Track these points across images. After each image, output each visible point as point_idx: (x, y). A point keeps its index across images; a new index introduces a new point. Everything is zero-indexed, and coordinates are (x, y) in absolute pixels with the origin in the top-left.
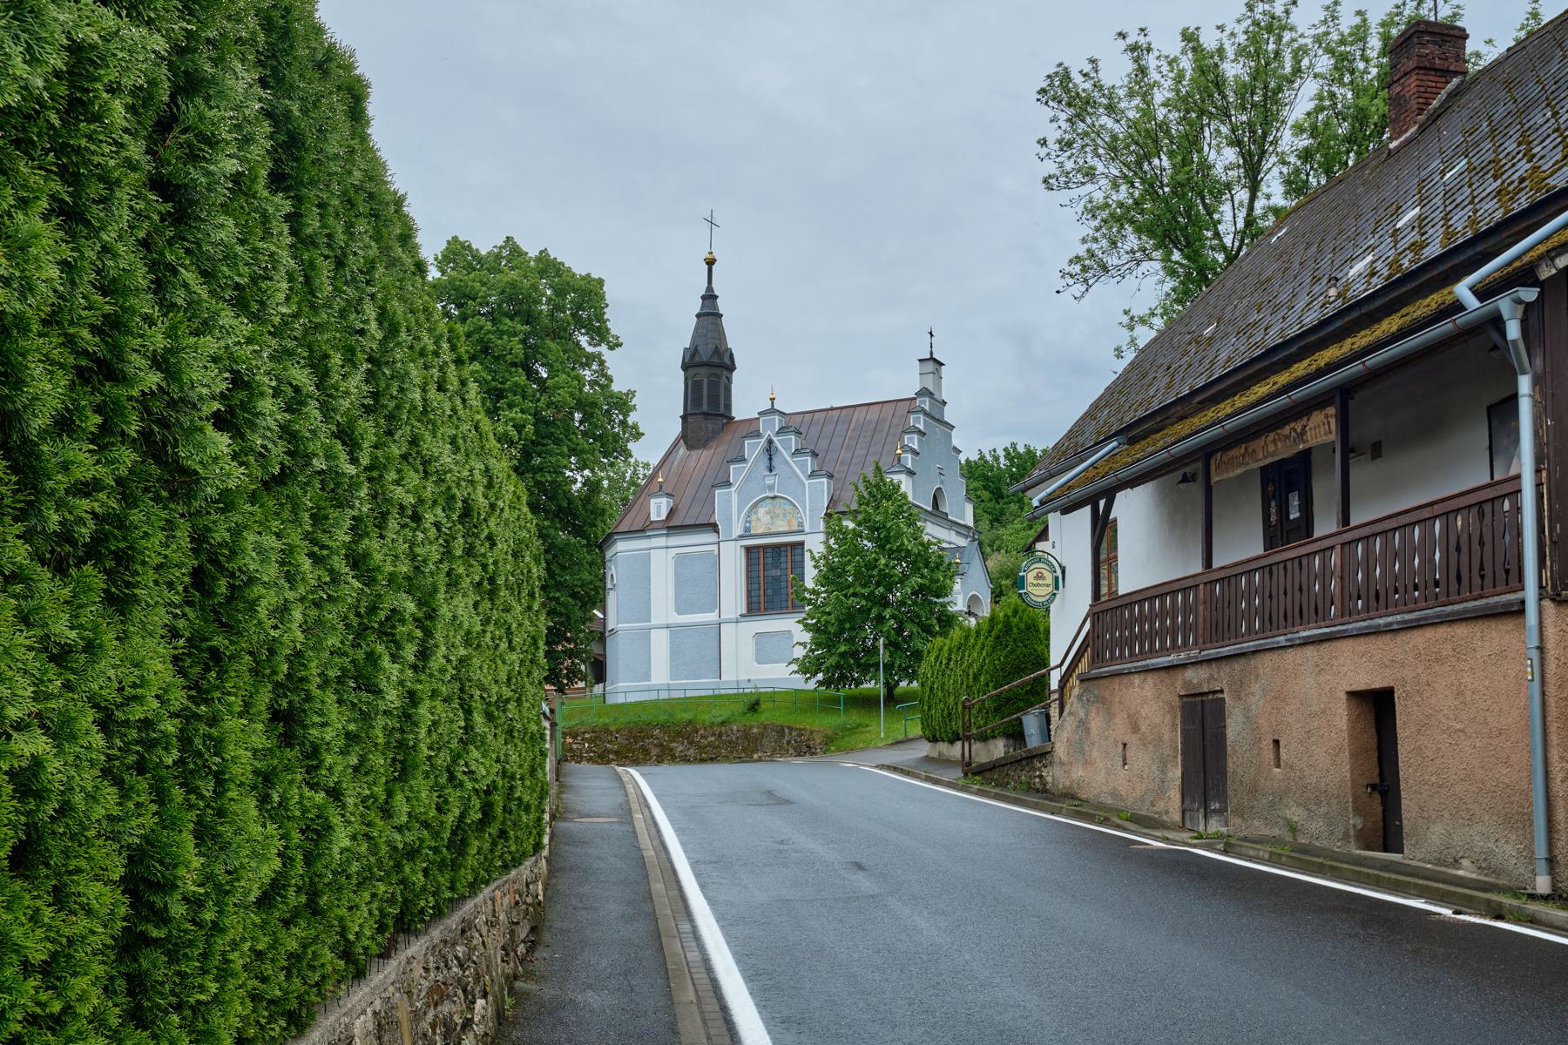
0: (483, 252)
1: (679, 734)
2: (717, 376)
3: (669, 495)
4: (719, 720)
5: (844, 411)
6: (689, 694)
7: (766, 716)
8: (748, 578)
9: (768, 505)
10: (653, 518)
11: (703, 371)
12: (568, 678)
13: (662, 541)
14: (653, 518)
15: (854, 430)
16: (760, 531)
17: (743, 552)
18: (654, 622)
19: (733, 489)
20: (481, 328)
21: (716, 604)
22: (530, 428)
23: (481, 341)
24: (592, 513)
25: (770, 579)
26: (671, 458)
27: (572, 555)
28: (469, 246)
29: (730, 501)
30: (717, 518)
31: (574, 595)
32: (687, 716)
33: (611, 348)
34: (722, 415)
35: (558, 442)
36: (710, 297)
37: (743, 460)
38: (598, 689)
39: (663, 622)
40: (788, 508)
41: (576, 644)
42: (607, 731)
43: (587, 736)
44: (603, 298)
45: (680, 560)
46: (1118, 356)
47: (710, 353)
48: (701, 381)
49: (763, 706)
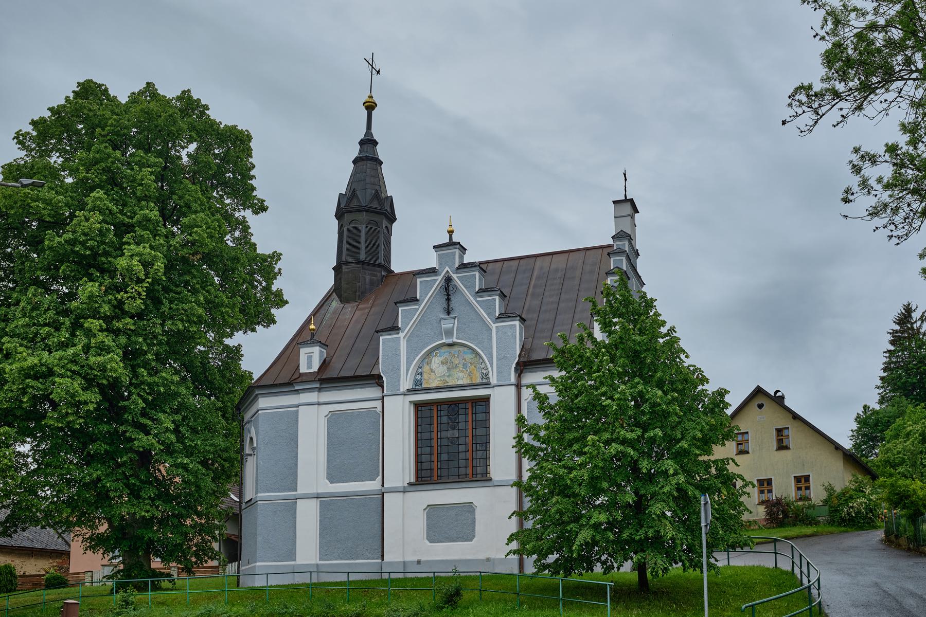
0: (123, 99)
2: (377, 224)
3: (323, 345)
6: (353, 577)
8: (417, 440)
9: (445, 353)
10: (303, 369)
11: (363, 217)
12: (196, 554)
13: (313, 397)
14: (303, 369)
15: (538, 278)
16: (434, 385)
18: (301, 490)
19: (401, 335)
21: (376, 469)
22: (159, 265)
23: (107, 170)
24: (230, 381)
25: (445, 442)
26: (322, 311)
28: (106, 90)
31: (204, 463)
34: (381, 266)
35: (194, 292)
36: (368, 142)
37: (414, 300)
38: (232, 568)
40: (469, 357)
41: (208, 519)
44: (248, 152)
45: (334, 420)
46: (846, 201)
48: (359, 228)
49: (466, 596)
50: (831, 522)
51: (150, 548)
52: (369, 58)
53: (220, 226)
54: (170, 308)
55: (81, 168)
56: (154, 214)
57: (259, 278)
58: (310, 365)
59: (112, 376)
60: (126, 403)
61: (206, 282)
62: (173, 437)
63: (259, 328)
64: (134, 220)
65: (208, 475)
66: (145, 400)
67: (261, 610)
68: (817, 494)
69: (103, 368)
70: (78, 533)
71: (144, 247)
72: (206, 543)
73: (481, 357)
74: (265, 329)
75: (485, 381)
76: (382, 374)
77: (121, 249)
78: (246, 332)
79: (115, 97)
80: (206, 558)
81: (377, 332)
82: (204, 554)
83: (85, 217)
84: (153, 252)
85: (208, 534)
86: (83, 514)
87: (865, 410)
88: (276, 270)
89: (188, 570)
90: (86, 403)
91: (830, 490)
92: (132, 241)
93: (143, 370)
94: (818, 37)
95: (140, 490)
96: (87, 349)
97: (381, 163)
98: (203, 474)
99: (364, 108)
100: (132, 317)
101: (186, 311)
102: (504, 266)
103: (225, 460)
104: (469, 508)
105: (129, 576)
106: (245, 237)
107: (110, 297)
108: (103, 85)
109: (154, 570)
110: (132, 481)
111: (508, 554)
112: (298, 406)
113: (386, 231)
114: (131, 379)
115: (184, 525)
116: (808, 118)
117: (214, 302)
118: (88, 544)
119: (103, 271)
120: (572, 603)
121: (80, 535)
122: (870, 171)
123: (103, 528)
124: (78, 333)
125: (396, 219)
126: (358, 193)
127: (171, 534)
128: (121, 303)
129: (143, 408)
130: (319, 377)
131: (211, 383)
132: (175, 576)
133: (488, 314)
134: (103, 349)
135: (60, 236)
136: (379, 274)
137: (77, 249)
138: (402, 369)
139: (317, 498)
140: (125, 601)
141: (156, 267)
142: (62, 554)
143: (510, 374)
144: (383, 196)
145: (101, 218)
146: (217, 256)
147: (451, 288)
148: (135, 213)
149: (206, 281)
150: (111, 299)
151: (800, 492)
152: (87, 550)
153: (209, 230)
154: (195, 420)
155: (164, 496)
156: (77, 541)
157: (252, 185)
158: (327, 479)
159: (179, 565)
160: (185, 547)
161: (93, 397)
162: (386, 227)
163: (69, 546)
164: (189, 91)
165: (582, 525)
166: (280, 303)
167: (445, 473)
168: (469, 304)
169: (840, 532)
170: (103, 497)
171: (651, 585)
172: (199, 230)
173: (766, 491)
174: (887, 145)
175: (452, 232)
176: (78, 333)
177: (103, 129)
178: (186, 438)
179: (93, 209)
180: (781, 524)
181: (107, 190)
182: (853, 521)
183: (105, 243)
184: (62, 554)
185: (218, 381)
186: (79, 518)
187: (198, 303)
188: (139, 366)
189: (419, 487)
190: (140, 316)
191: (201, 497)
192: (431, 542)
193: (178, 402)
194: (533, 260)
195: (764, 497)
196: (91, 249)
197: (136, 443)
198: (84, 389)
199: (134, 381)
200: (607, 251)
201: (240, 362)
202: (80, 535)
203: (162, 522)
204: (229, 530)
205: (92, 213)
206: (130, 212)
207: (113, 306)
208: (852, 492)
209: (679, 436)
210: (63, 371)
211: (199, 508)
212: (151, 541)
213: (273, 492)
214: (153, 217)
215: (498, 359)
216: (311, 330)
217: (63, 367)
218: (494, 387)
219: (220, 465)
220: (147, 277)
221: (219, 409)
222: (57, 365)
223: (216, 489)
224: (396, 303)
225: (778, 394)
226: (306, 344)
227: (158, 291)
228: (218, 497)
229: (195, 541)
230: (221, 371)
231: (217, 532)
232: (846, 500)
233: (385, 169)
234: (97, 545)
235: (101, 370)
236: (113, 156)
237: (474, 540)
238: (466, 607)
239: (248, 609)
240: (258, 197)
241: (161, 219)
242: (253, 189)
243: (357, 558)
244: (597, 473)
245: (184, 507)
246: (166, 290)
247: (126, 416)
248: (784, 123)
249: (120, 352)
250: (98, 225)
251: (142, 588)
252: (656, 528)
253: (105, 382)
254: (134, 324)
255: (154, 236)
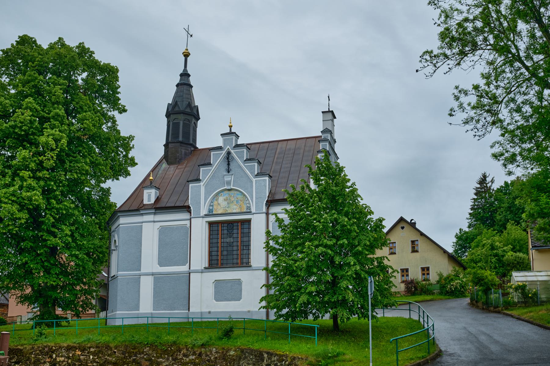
0: (45, 46)
1: (165, 352)
2: (189, 121)
3: (157, 188)
4: (200, 343)
5: (271, 144)
6: (172, 321)
7: (242, 342)
8: (210, 243)
9: (226, 195)
10: (146, 202)
11: (181, 117)
12: (82, 306)
13: (151, 218)
14: (146, 202)
15: (279, 153)
16: (220, 212)
17: (207, 224)
18: (143, 270)
19: (202, 184)
20: (36, 78)
21: (186, 259)
22: (64, 141)
23: (35, 86)
27: (89, 229)
28: (35, 41)
29: (200, 191)
30: (190, 202)
31: (88, 254)
32: (171, 338)
33: (120, 113)
34: (191, 145)
35: (84, 157)
36: (185, 75)
37: (209, 164)
38: (102, 315)
39: (150, 271)
40: (240, 197)
41: (89, 286)
42: (108, 347)
43: (92, 350)
45: (163, 231)
46: (451, 115)
47: (184, 106)
49: (236, 332)
50: (441, 293)
51: (56, 302)
52: (186, 28)
53: (99, 120)
54: (70, 166)
55: (20, 85)
56: (62, 112)
57: (121, 150)
58: (149, 200)
59: (35, 204)
60: (43, 219)
61: (91, 151)
62: (70, 239)
63: (121, 178)
64: (50, 115)
65: (90, 261)
66: (54, 218)
67: (119, 339)
68: (433, 277)
69: (30, 199)
70: (13, 293)
71: (56, 131)
72: (88, 300)
73: (246, 197)
74: (125, 179)
75: (248, 210)
76: (190, 205)
77: (42, 131)
78: (113, 180)
79: (40, 45)
80: (88, 309)
81: (188, 182)
82: (86, 306)
83: (22, 112)
84: (61, 134)
85: (89, 294)
86: (17, 282)
87: (460, 231)
88: (131, 146)
89: (78, 315)
90: (20, 219)
91: (440, 275)
92: (48, 127)
93: (53, 200)
94: (436, 25)
95: (50, 269)
96: (21, 188)
97: (192, 87)
98: (87, 261)
99: (183, 56)
100: (48, 170)
101: (79, 167)
102: (261, 146)
103: (100, 253)
104: (238, 282)
105: (43, 319)
106: (114, 126)
107: (35, 159)
108: (33, 38)
109: (57, 315)
110: (46, 264)
111: (260, 309)
112: (142, 223)
113: (194, 125)
114: (46, 206)
115: (75, 289)
116: (431, 68)
117: (95, 163)
118: (19, 300)
119: (31, 144)
120: (296, 336)
121: (15, 294)
122: (464, 99)
123: (28, 291)
124: (16, 179)
125: (200, 118)
126: (178, 103)
127: (68, 294)
128: (41, 162)
129: (53, 222)
130: (154, 207)
131: (92, 208)
132: (70, 319)
133: (251, 173)
134: (30, 188)
135: (6, 123)
136: (189, 149)
137: (16, 131)
138: (201, 203)
139: (152, 275)
140: (40, 333)
141: (62, 142)
142: (4, 305)
143: (263, 207)
144: (193, 106)
145: (31, 113)
146: (98, 137)
147: (230, 158)
148: (51, 111)
149: (91, 151)
150: (36, 160)
151: (424, 276)
152: (18, 303)
153: (93, 122)
154: (83, 230)
155: (65, 273)
156: (13, 298)
157: (118, 97)
158: (158, 264)
159: (72, 313)
160: (76, 302)
161: (24, 216)
162: (194, 123)
163: (8, 301)
164: (83, 43)
165: (302, 293)
166: (133, 164)
167: (225, 262)
168: (240, 167)
169: (446, 299)
170: (29, 272)
171: (340, 327)
172: (87, 122)
173: (405, 275)
174: (473, 85)
175: (231, 126)
176: (16, 179)
177: (33, 63)
178: (78, 240)
179: (26, 108)
180: (413, 294)
181: (35, 98)
182: (454, 293)
183: (33, 128)
184: (4, 305)
185: (97, 207)
186: (14, 285)
187: (86, 163)
188: (51, 198)
189: (210, 270)
190: (53, 169)
191: (85, 274)
192: (216, 301)
193: (74, 219)
194: (276, 143)
195: (404, 278)
196: (25, 131)
197: (49, 242)
198: (19, 211)
199: (48, 207)
200: (318, 139)
201: (110, 197)
202: (15, 294)
203: (63, 288)
204: (102, 293)
205: (25, 111)
206: (48, 110)
207: (37, 163)
208: (452, 277)
209: (357, 244)
210: (6, 200)
211: (84, 280)
212: (56, 299)
213: (127, 271)
214: (61, 114)
215: (256, 198)
216: (150, 180)
217: (6, 198)
218: (253, 214)
219: (97, 255)
220: (57, 148)
221: (97, 223)
222: (4, 197)
223: (94, 269)
224: (199, 166)
225: (413, 221)
226: (147, 187)
227: (63, 156)
228: (95, 274)
229: (82, 299)
230: (98, 202)
231: (94, 294)
232: (449, 281)
233: (194, 90)
234: (24, 300)
235: (29, 200)
236: (39, 78)
237: (241, 300)
238: (236, 339)
239: (112, 338)
240: (122, 104)
241: (66, 115)
242: (119, 99)
243: (175, 310)
244: (311, 263)
245: (76, 279)
246: (68, 155)
247: (43, 227)
248: (417, 71)
249: (40, 190)
250: (29, 118)
251: (50, 325)
252: (343, 295)
253: (31, 207)
254: (49, 174)
255: (62, 125)
